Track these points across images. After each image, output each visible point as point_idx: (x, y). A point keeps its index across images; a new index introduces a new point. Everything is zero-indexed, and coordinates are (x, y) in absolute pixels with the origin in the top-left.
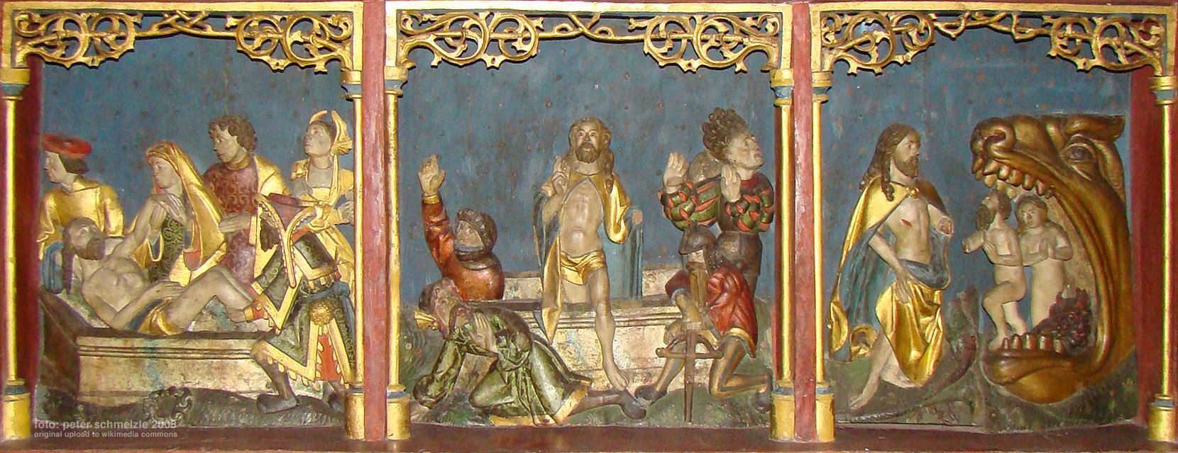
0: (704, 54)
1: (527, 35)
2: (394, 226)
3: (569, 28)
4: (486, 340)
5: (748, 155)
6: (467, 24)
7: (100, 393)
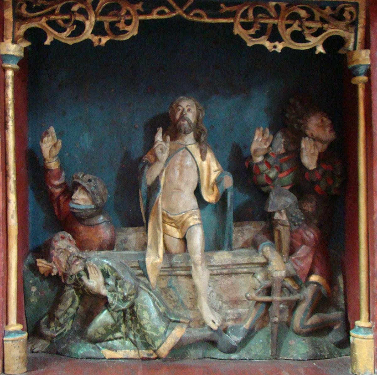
0: (288, 37)
1: (129, 18)
2: (12, 185)
3: (167, 10)
4: (229, 269)
5: (324, 130)
6: (75, 8)
7: (92, 291)
